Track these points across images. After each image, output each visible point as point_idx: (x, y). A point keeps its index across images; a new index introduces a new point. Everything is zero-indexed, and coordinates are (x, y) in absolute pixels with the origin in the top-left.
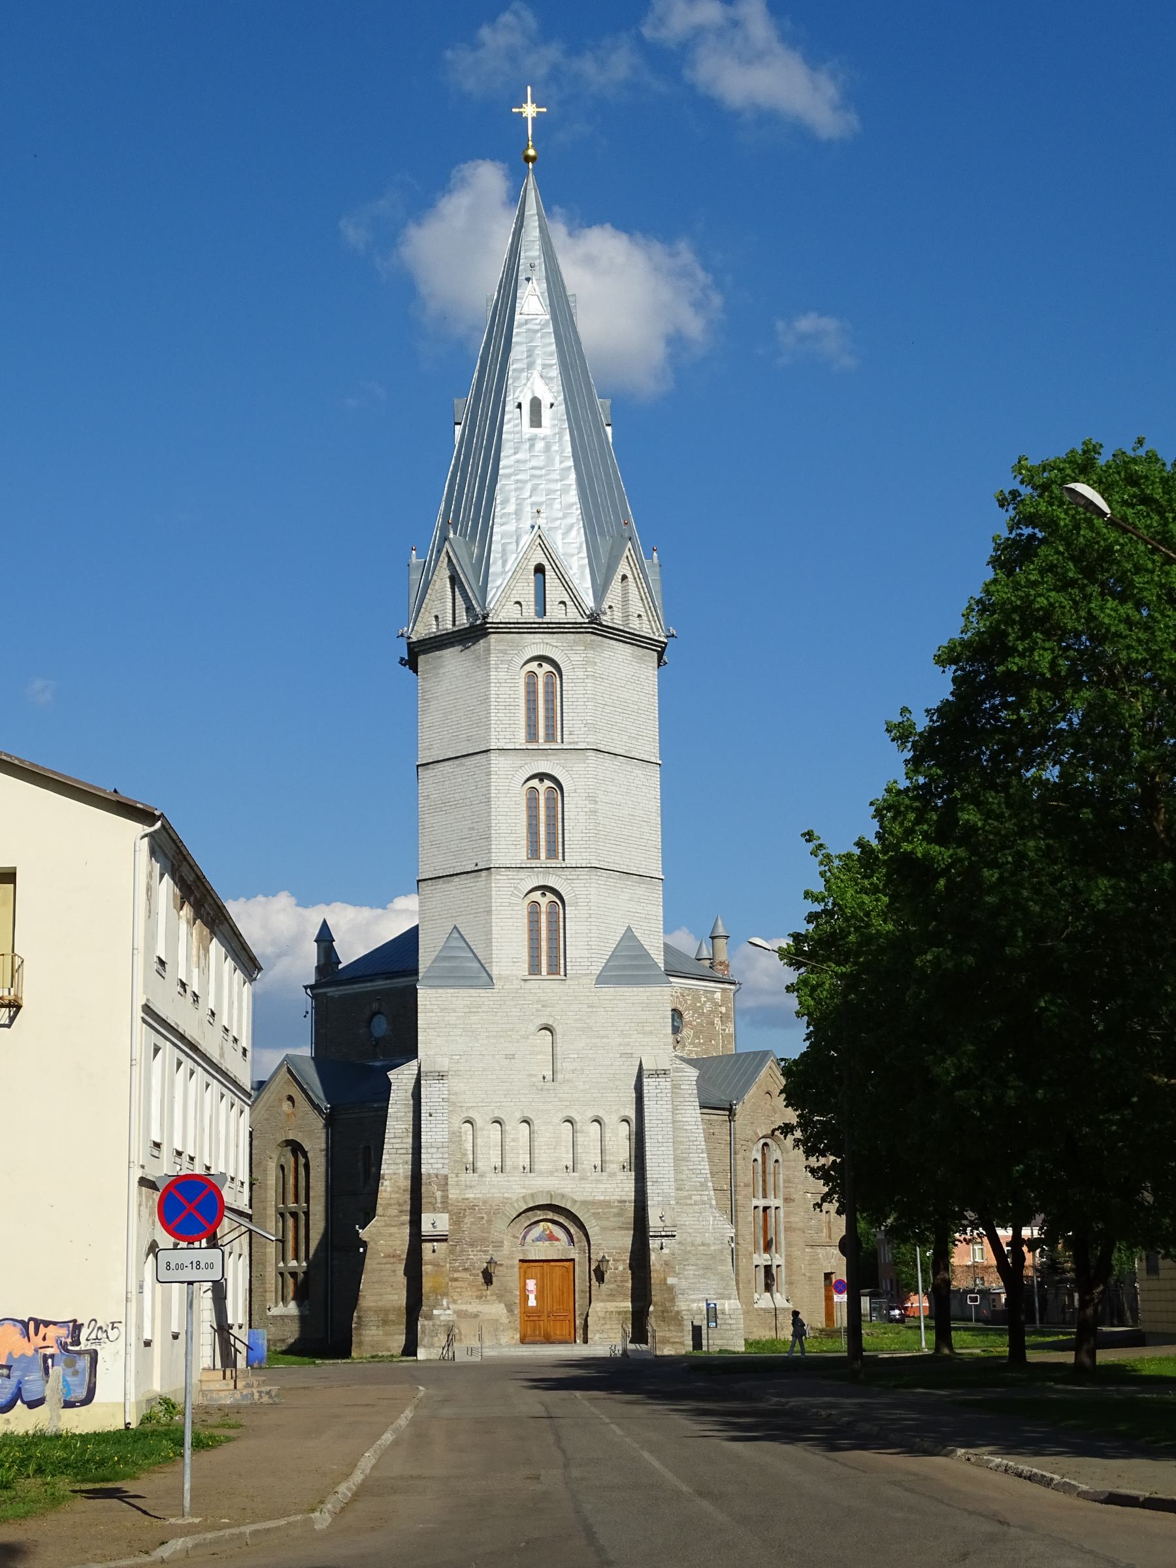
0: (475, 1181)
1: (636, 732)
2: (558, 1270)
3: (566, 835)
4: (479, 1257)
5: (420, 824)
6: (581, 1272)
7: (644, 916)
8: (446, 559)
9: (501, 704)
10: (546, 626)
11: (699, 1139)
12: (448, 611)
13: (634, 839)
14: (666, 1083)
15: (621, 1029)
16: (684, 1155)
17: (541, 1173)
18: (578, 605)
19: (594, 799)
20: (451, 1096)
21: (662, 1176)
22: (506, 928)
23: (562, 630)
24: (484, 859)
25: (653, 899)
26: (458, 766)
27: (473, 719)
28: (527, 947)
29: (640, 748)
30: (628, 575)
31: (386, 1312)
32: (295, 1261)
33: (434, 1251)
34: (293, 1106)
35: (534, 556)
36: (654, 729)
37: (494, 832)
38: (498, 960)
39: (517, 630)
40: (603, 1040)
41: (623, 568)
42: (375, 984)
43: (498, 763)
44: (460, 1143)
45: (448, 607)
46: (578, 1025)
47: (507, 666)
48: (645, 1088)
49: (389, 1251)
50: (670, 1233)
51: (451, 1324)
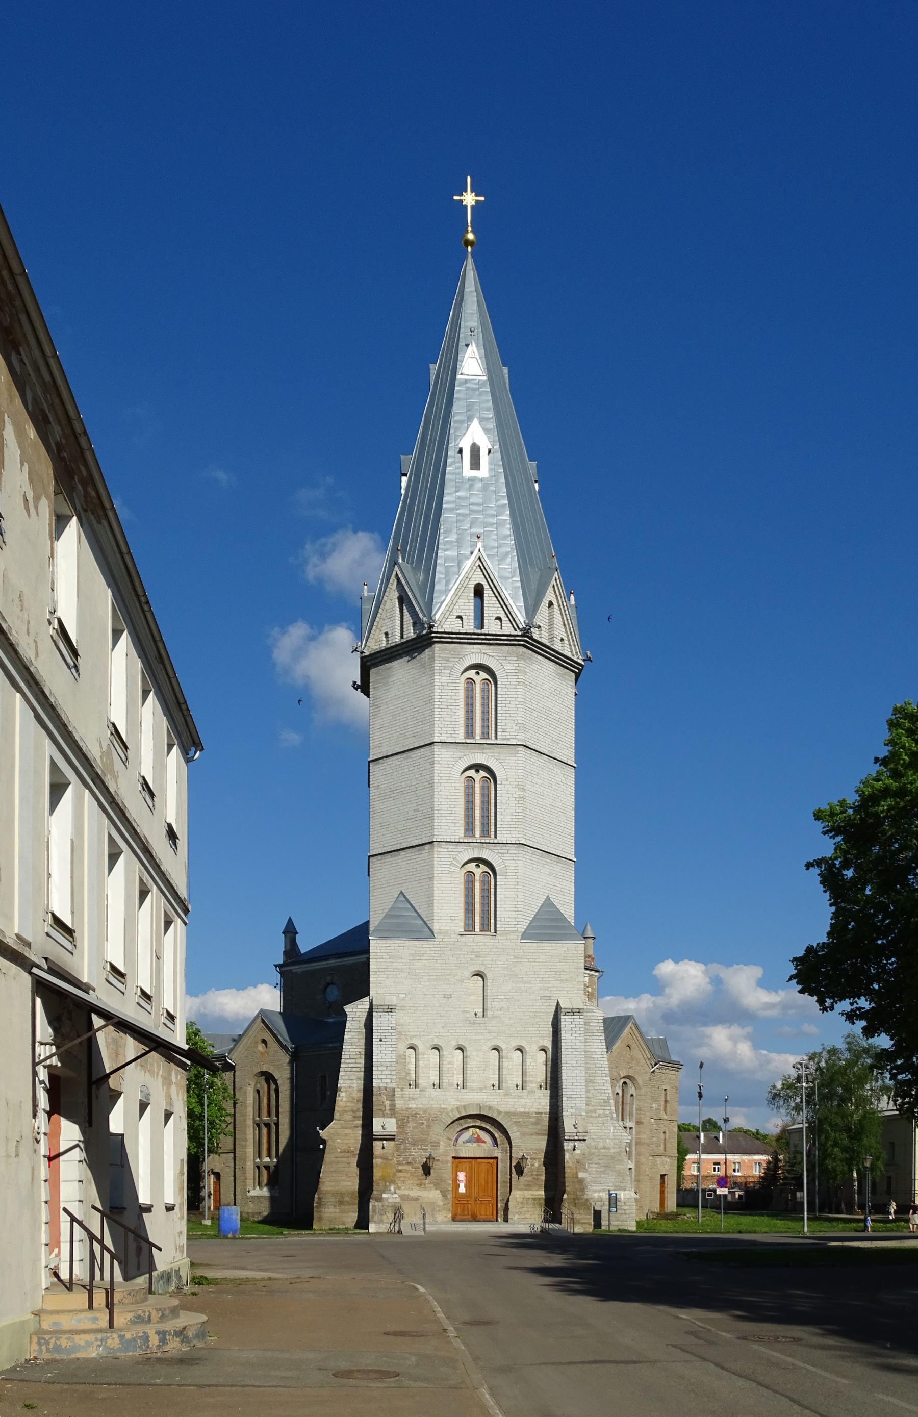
0: (417, 1094)
1: (557, 737)
2: (484, 1165)
3: (498, 816)
4: (419, 1154)
5: (371, 810)
6: (503, 1167)
7: (560, 889)
8: (396, 581)
9: (443, 704)
10: (484, 637)
11: (603, 1065)
12: (396, 627)
13: (554, 825)
14: (580, 1020)
15: (541, 976)
16: (591, 1078)
17: (472, 1090)
18: (512, 620)
19: (522, 787)
20: (397, 1027)
21: (575, 1093)
22: (446, 892)
23: (498, 642)
24: (427, 835)
25: (567, 876)
26: (404, 759)
27: (418, 718)
28: (463, 908)
29: (560, 751)
30: (554, 603)
31: (342, 1194)
32: (268, 1158)
33: (383, 1148)
34: (266, 1047)
35: (474, 576)
36: (570, 737)
37: (437, 812)
38: (439, 918)
39: (488, 637)
40: (526, 985)
41: (550, 596)
42: (328, 962)
43: (441, 754)
44: (405, 1064)
45: (397, 624)
46: (506, 972)
47: (449, 671)
48: (562, 1023)
49: (345, 1147)
50: (582, 1138)
51: (397, 1205)
